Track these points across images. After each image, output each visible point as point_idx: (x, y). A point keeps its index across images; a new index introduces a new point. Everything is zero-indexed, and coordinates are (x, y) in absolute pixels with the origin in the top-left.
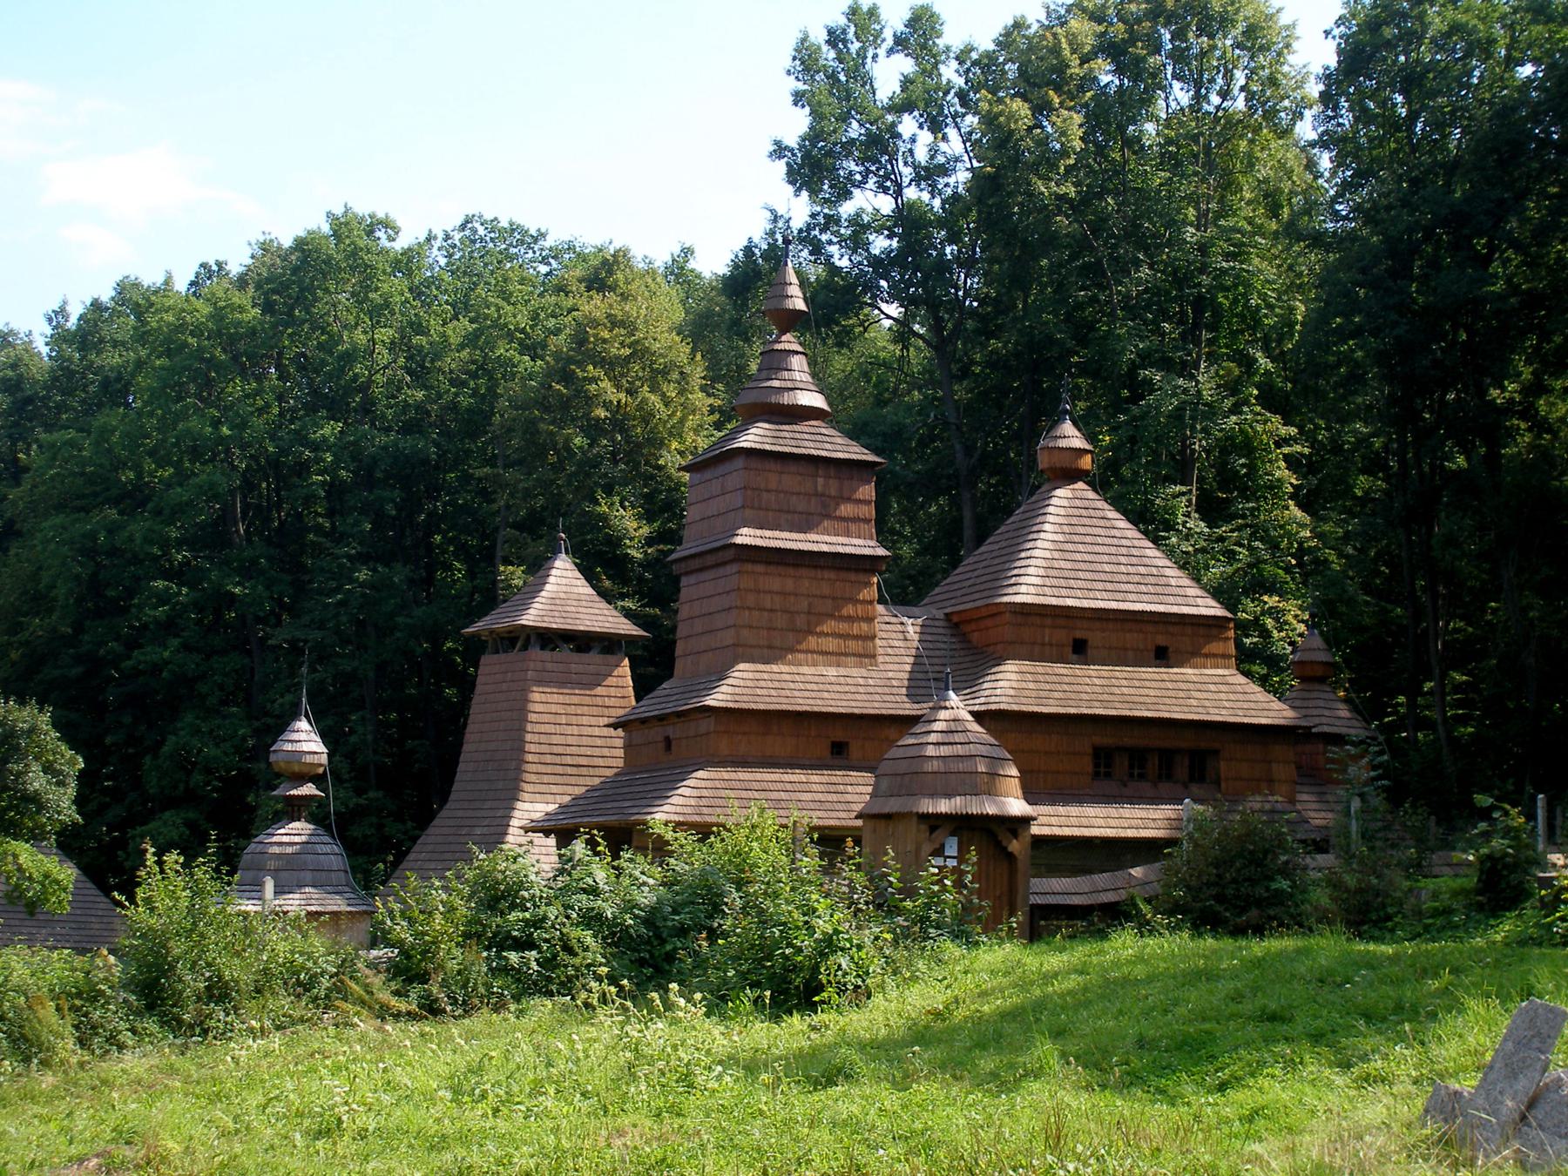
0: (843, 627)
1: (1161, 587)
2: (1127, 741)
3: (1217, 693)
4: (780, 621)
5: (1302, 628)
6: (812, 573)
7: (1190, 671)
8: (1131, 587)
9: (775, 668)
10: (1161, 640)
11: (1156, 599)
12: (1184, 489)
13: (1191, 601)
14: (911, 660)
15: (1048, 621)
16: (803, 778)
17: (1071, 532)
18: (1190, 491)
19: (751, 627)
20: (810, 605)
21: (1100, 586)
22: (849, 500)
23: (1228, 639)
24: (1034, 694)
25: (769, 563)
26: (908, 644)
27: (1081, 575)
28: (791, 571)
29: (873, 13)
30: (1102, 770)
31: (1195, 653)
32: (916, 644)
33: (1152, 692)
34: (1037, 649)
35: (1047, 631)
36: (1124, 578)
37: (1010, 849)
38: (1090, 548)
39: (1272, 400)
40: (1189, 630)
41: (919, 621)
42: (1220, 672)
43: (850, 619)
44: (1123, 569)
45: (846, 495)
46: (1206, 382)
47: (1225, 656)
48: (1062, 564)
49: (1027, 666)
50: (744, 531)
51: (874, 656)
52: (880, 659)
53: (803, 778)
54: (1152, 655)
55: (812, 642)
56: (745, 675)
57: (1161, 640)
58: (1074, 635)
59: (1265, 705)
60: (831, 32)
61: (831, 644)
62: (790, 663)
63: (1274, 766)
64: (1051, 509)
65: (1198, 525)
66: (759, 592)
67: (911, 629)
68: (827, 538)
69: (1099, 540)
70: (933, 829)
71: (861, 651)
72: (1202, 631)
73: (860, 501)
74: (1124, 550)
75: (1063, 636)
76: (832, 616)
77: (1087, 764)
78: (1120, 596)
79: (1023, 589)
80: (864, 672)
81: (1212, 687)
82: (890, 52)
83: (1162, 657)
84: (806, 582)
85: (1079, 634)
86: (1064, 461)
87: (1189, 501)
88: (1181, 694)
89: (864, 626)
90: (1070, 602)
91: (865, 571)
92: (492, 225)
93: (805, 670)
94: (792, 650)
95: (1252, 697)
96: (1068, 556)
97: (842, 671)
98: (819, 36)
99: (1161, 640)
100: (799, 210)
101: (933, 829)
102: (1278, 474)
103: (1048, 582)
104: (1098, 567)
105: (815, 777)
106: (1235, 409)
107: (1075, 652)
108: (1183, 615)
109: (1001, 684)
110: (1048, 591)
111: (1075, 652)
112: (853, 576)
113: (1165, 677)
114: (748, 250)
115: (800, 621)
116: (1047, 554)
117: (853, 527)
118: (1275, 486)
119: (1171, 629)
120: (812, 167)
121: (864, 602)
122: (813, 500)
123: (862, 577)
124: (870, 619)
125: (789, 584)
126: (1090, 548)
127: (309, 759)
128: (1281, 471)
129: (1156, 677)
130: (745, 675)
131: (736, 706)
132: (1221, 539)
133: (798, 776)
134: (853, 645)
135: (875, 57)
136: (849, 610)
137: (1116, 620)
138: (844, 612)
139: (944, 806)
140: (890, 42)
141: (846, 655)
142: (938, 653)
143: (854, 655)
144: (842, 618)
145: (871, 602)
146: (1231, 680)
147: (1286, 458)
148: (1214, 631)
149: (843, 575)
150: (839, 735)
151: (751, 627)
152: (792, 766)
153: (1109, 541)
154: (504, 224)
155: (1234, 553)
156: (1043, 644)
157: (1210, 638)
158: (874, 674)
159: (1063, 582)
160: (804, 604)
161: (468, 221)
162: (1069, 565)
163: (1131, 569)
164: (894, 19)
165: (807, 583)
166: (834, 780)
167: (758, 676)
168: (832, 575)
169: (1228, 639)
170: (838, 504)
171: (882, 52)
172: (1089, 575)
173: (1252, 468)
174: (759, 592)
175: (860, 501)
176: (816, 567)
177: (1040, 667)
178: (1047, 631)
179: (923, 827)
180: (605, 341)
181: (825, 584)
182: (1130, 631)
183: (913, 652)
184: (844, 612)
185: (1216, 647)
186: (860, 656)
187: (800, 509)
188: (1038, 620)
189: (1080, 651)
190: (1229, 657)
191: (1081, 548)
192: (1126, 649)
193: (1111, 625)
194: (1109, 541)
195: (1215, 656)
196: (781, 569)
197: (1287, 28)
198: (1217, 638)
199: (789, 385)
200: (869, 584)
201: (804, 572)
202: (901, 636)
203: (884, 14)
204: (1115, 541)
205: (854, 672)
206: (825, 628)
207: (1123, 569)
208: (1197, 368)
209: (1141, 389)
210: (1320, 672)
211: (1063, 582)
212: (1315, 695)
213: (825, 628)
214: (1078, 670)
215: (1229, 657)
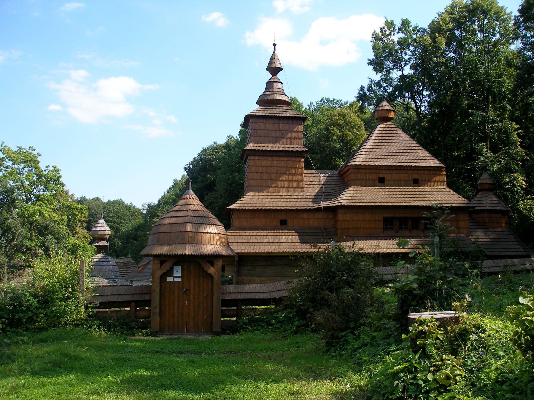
0: (291, 178)
1: (417, 157)
2: (398, 215)
3: (439, 195)
4: (265, 176)
5: (524, 182)
6: (277, 158)
7: (427, 188)
8: (403, 157)
9: (262, 194)
10: (416, 176)
11: (413, 161)
12: (485, 144)
13: (428, 161)
14: (319, 189)
15: (368, 171)
16: (266, 234)
17: (382, 139)
18: (487, 144)
19: (253, 179)
20: (277, 171)
21: (390, 157)
22: (292, 131)
23: (443, 175)
24: (359, 198)
25: (260, 156)
26: (320, 183)
27: (383, 154)
28: (269, 158)
29: (392, 22)
30: (389, 227)
31: (430, 181)
32: (323, 183)
33: (409, 196)
34: (363, 182)
35: (368, 175)
36: (401, 154)
37: (209, 272)
38: (388, 144)
39: (512, 118)
40: (427, 172)
41: (327, 175)
42: (440, 187)
43: (293, 174)
44: (401, 151)
45: (291, 130)
46: (491, 112)
47: (441, 181)
48: (376, 150)
49: (359, 188)
50: (251, 144)
51: (303, 188)
52: (305, 189)
53: (266, 234)
54: (412, 182)
55: (278, 183)
56: (249, 197)
57: (415, 176)
58: (380, 176)
59: (456, 199)
60: (381, 29)
61: (285, 184)
62: (269, 192)
63: (460, 222)
64: (376, 132)
65: (489, 153)
66: (256, 166)
67: (322, 178)
68: (283, 146)
69: (393, 141)
70: (162, 263)
71: (297, 186)
72: (432, 172)
73: (297, 132)
74: (403, 145)
75: (374, 176)
76: (286, 174)
77: (381, 224)
78: (398, 161)
79: (358, 160)
80: (298, 194)
81: (435, 193)
82: (398, 33)
83: (416, 182)
84: (276, 162)
85: (381, 175)
86: (383, 114)
87: (487, 148)
88: (422, 196)
89: (299, 177)
90: (376, 164)
91: (298, 157)
92: (328, 100)
93: (275, 194)
94: (270, 187)
95: (452, 196)
96: (379, 147)
97: (289, 194)
98: (378, 31)
99: (416, 176)
100: (377, 77)
101: (162, 263)
102: (514, 139)
103: (369, 157)
104: (391, 151)
105: (271, 233)
106: (501, 121)
107: (379, 182)
108: (424, 167)
109: (346, 195)
110: (368, 160)
111: (379, 182)
112: (294, 159)
113: (416, 190)
114: (362, 88)
115: (273, 176)
116: (371, 147)
117: (294, 141)
118: (514, 142)
119: (419, 172)
120: (377, 65)
121: (298, 168)
122: (278, 132)
123: (297, 159)
124: (301, 174)
125: (269, 163)
126: (388, 144)
127: (100, 233)
128: (516, 138)
129: (413, 190)
130: (249, 197)
131: (240, 208)
132: (496, 157)
133: (265, 233)
134: (294, 184)
135: (394, 34)
136: (293, 171)
137: (396, 170)
138: (291, 172)
139: (164, 250)
140: (397, 30)
141: (292, 188)
142: (331, 186)
143: (295, 188)
144: (290, 174)
145: (301, 168)
146: (443, 190)
147: (518, 134)
148: (437, 172)
149: (290, 159)
150: (283, 217)
151: (253, 179)
152: (262, 229)
153: (397, 141)
154: (343, 102)
155: (500, 161)
156: (366, 180)
157: (436, 175)
158: (302, 194)
159: (375, 157)
160: (275, 170)
161: (322, 99)
162: (379, 150)
163: (404, 151)
164: (398, 24)
165: (275, 162)
166: (279, 234)
167: (254, 197)
168: (286, 159)
169: (443, 175)
170: (288, 133)
171: (396, 33)
172: (386, 154)
173: (507, 137)
174: (256, 166)
175: (297, 132)
176: (279, 156)
177: (364, 189)
178: (368, 175)
179: (157, 262)
180: (337, 120)
181: (283, 162)
182: (403, 173)
183: (321, 186)
184: (291, 172)
185: (439, 178)
186: (297, 188)
187: (273, 135)
188: (364, 171)
189: (382, 182)
190: (444, 182)
191: (385, 144)
192: (401, 180)
193: (394, 172)
194: (397, 141)
195: (438, 181)
196: (266, 158)
197: (509, 14)
198: (439, 175)
199: (272, 93)
200: (300, 161)
201: (275, 158)
202: (318, 180)
203: (395, 22)
204: (400, 141)
205: (294, 194)
206: (283, 178)
207: (401, 151)
208: (488, 109)
209: (469, 115)
210: (487, 187)
211: (375, 157)
212: (485, 195)
213: (283, 178)
214: (380, 189)
215: (444, 182)
